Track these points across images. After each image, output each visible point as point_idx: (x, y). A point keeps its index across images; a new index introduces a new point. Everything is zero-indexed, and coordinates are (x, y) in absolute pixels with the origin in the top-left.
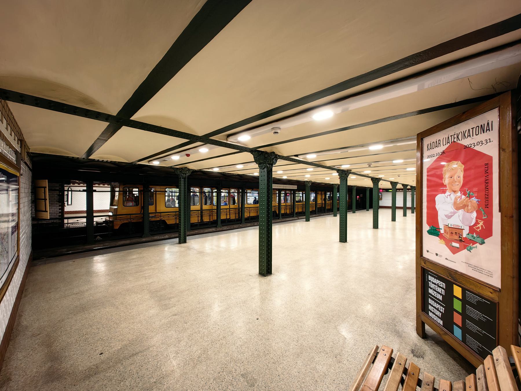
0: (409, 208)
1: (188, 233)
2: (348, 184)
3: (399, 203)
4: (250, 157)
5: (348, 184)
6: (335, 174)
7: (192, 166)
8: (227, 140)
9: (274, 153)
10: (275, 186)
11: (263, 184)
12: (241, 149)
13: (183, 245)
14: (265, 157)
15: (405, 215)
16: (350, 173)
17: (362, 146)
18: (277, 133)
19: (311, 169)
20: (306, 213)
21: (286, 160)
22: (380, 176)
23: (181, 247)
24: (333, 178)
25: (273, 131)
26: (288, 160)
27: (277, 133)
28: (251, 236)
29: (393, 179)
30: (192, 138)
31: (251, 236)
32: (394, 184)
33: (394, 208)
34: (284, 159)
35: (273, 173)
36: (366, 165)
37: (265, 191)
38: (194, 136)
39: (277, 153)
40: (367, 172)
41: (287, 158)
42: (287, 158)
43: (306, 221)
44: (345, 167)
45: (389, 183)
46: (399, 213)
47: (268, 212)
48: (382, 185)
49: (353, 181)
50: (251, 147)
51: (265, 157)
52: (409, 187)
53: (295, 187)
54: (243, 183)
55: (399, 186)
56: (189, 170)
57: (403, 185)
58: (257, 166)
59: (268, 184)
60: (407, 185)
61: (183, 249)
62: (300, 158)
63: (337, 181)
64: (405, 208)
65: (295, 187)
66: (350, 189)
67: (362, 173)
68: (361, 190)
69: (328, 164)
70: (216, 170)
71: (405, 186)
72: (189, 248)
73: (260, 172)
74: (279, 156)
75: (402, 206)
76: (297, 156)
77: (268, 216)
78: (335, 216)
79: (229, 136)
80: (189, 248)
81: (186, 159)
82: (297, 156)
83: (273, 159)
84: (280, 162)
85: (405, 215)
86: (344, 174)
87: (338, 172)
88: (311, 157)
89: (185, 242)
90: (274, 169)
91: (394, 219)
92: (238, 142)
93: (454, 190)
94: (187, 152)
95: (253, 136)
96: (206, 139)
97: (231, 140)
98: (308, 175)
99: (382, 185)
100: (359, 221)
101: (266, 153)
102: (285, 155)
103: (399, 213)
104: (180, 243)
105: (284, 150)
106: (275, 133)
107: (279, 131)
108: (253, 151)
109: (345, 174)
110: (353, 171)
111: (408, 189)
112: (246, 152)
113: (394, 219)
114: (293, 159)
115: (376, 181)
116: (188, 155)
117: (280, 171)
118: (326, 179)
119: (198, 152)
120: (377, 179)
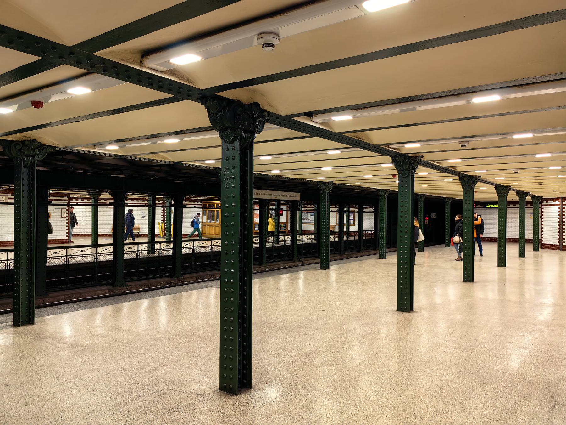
0: (529, 241)
1: (36, 302)
2: (416, 192)
3: (512, 232)
4: (195, 113)
5: (416, 192)
6: (387, 165)
7: (47, 137)
8: (141, 64)
9: (257, 105)
10: (258, 194)
11: (231, 184)
12: (178, 90)
13: (23, 329)
14: (236, 115)
15: (522, 254)
16: (478, 181)
17: (457, 94)
18: (271, 45)
19: (336, 151)
20: (323, 252)
21: (285, 126)
22: (478, 172)
23: (20, 334)
24: (379, 174)
25: (262, 41)
26: (290, 127)
27: (271, 45)
28: (203, 303)
29: (501, 180)
30: (47, 53)
31: (203, 303)
32: (502, 190)
33: (502, 241)
34: (279, 124)
35: (256, 161)
36: (456, 144)
37: (236, 203)
38: (54, 46)
39: (265, 106)
40: (454, 161)
41: (287, 122)
42: (287, 122)
43: (322, 268)
44: (410, 148)
45: (493, 188)
46: (512, 251)
47: (242, 251)
48: (484, 192)
49: (426, 182)
50: (203, 85)
51: (236, 115)
52: (529, 198)
53: (296, 196)
54: (172, 183)
55: (512, 196)
56: (42, 146)
57: (519, 193)
58: (214, 137)
59: (237, 188)
60: (526, 194)
61: (23, 339)
62: (317, 122)
63: (394, 184)
64: (521, 242)
65: (296, 196)
66: (417, 198)
67: (444, 164)
68: (434, 205)
69: (376, 138)
70: (112, 148)
71: (521, 194)
72: (41, 337)
73: (225, 158)
74: (269, 113)
75: (496, 235)
76: (310, 115)
77: (242, 261)
78: (383, 257)
79: (147, 53)
80: (41, 337)
81: (32, 117)
82: (310, 115)
83: (255, 120)
84: (270, 131)
85: (522, 254)
86: (406, 164)
87: (394, 161)
88: (342, 120)
89: (328, 268)
90: (257, 148)
91: (502, 263)
92: (172, 72)
93: (269, 49)
94: (36, 96)
95: (207, 57)
96: (87, 58)
97: (153, 66)
98: (329, 165)
99: (484, 192)
100: (437, 268)
101: (238, 103)
102: (283, 112)
103: (512, 251)
104: (16, 324)
105: (282, 97)
106: (266, 45)
107: (275, 42)
108: (210, 98)
109: (411, 164)
110: (427, 158)
111: (528, 203)
112: (188, 102)
113: (502, 263)
114: (300, 123)
115: (469, 182)
116: (38, 104)
117: (274, 154)
118: (366, 177)
119: (64, 92)
120: (471, 177)
